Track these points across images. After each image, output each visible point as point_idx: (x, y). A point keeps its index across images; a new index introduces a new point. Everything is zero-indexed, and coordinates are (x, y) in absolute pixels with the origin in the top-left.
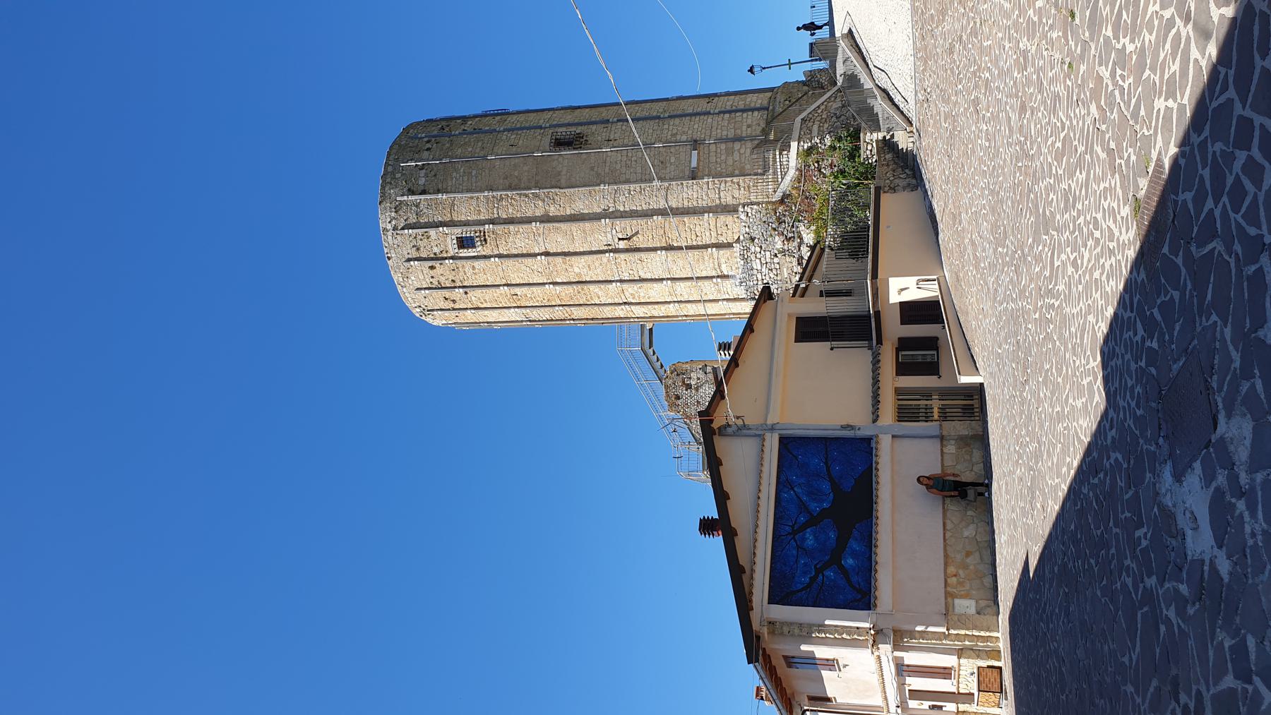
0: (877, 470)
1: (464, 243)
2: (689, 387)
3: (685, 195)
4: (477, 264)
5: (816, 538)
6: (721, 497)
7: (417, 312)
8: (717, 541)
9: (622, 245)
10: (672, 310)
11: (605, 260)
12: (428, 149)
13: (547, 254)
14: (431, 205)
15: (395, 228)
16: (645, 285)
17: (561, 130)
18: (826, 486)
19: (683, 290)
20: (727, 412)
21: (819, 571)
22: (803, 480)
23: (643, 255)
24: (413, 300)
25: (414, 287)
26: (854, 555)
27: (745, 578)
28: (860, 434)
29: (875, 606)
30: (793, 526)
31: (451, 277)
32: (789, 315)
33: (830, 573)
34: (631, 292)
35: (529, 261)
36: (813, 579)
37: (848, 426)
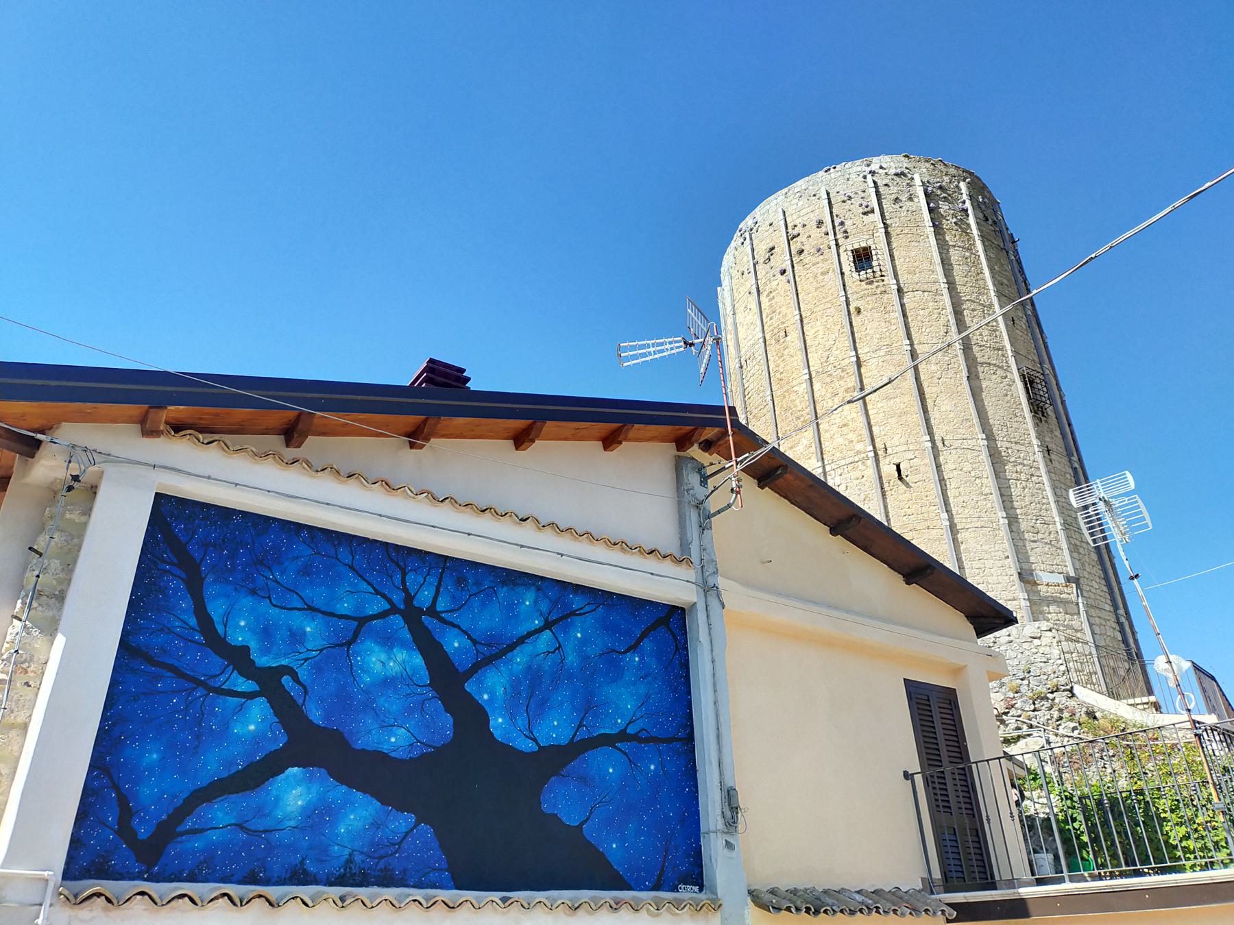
0: (615, 907)
1: (863, 258)
3: (989, 563)
5: (388, 683)
7: (749, 221)
11: (860, 447)
13: (859, 364)
15: (873, 173)
18: (555, 728)
21: (270, 683)
22: (571, 658)
26: (318, 817)
28: (714, 847)
29: (79, 901)
30: (432, 611)
31: (806, 248)
32: (958, 671)
33: (255, 721)
35: (848, 342)
36: (239, 658)
37: (735, 809)
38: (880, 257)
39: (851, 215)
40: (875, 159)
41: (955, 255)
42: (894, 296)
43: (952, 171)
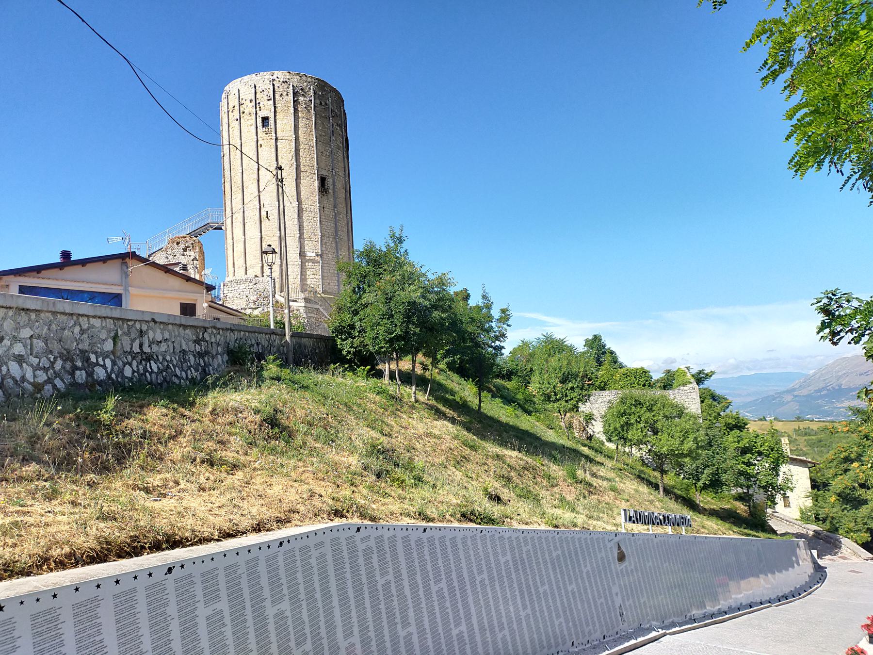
1: (265, 120)
2: (185, 250)
4: (254, 127)
6: (83, 262)
8: (57, 259)
9: (264, 214)
10: (229, 241)
12: (321, 103)
14: (286, 103)
16: (242, 226)
17: (331, 181)
19: (239, 248)
20: (134, 267)
23: (258, 225)
24: (233, 86)
25: (240, 87)
27: (35, 273)
34: (238, 217)
38: (272, 121)
39: (262, 98)
40: (276, 73)
41: (301, 123)
42: (274, 141)
43: (309, 80)
